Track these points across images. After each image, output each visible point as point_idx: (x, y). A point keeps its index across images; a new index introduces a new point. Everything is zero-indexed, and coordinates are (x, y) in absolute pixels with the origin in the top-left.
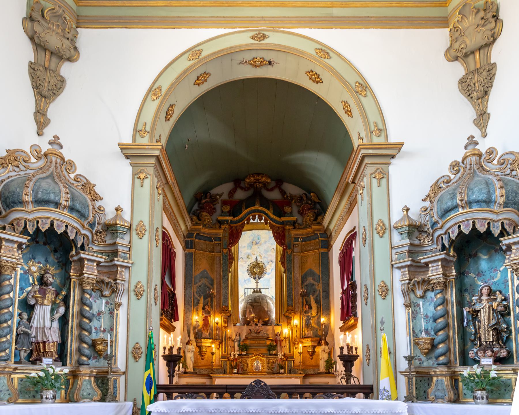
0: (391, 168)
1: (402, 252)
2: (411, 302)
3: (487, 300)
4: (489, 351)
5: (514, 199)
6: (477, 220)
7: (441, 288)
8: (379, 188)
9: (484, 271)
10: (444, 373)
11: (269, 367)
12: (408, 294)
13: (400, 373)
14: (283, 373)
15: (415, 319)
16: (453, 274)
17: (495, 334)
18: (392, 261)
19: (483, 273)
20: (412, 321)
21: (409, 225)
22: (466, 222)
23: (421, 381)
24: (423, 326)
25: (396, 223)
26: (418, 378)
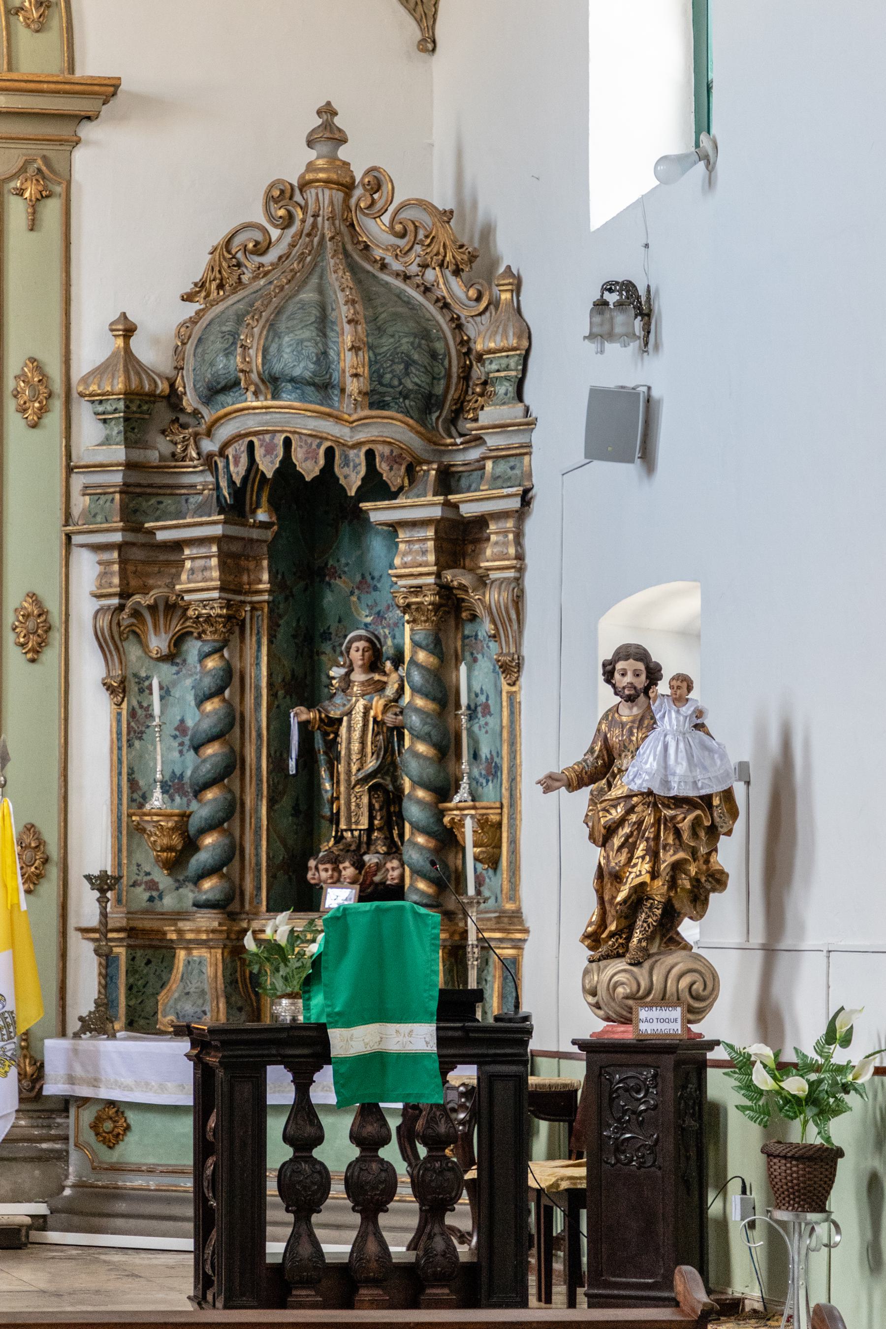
0: (79, 156)
2: (130, 677)
3: (363, 684)
4: (347, 864)
5: (400, 383)
6: (297, 436)
7: (216, 637)
8: (33, 235)
9: (376, 574)
10: (204, 937)
12: (117, 648)
13: (79, 934)
15: (140, 739)
16: (261, 586)
17: (377, 806)
18: (68, 515)
19: (375, 582)
21: (125, 394)
22: (267, 437)
23: (149, 962)
24: (159, 768)
25: (85, 380)
26: (139, 953)
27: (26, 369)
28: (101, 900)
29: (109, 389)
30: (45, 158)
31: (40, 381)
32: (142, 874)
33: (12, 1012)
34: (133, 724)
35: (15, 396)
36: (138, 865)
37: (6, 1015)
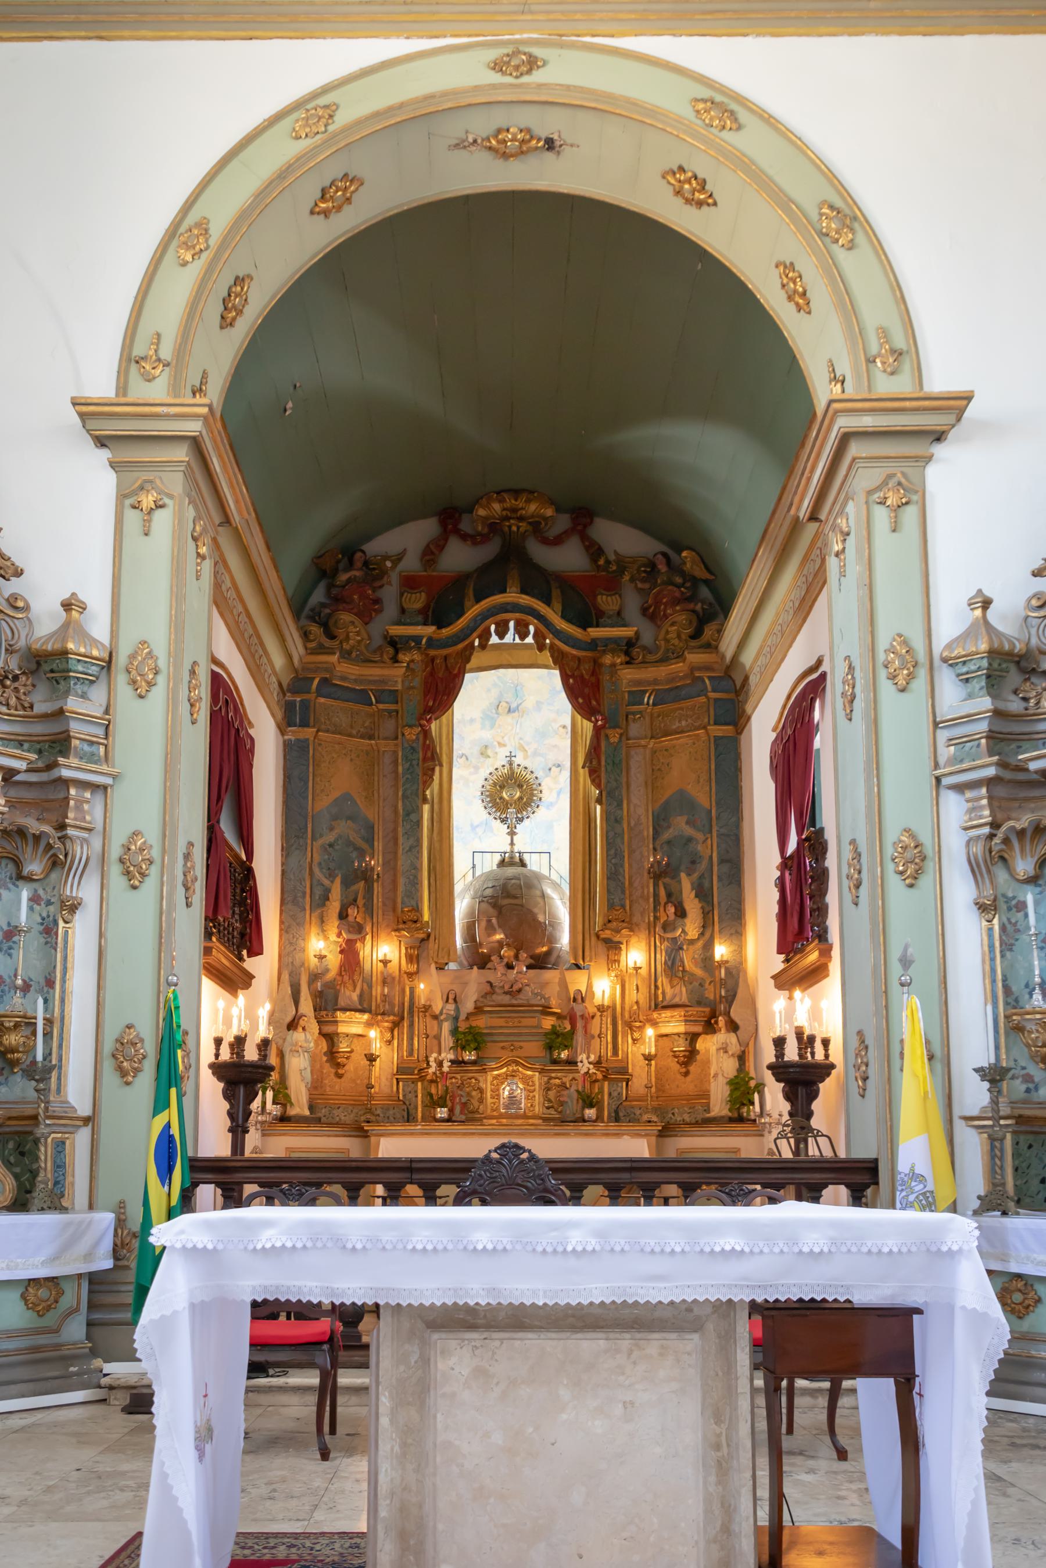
1: (970, 738)
2: (999, 896)
8: (894, 534)
11: (550, 1101)
12: (989, 871)
13: (963, 1122)
14: (595, 1121)
15: (1011, 950)
20: (1002, 956)
23: (1030, 1147)
24: (1037, 972)
26: (1022, 1138)
27: (895, 643)
28: (993, 1089)
29: (974, 649)
30: (904, 474)
31: (907, 652)
32: (1019, 1068)
33: (932, 1192)
34: (1004, 937)
35: (886, 667)
36: (1015, 1061)
37: (928, 1195)
